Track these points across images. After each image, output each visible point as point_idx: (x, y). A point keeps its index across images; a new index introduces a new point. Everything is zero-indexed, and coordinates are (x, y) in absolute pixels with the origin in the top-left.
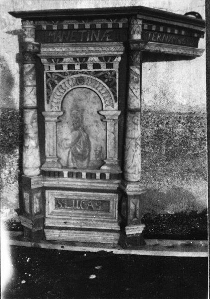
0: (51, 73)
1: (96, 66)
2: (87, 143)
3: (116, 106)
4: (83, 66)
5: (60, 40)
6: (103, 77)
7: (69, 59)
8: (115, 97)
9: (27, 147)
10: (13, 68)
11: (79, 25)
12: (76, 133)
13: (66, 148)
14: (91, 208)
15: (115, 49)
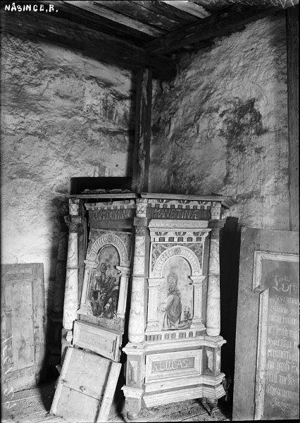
0: (157, 245)
1: (190, 239)
2: (179, 306)
3: (201, 271)
4: (180, 239)
5: (163, 217)
6: (193, 249)
7: (150, 166)
8: (201, 264)
9: (36, 375)
10: (10, 149)
11: (179, 206)
12: (171, 297)
13: (163, 312)
14: (179, 368)
15: (205, 223)
